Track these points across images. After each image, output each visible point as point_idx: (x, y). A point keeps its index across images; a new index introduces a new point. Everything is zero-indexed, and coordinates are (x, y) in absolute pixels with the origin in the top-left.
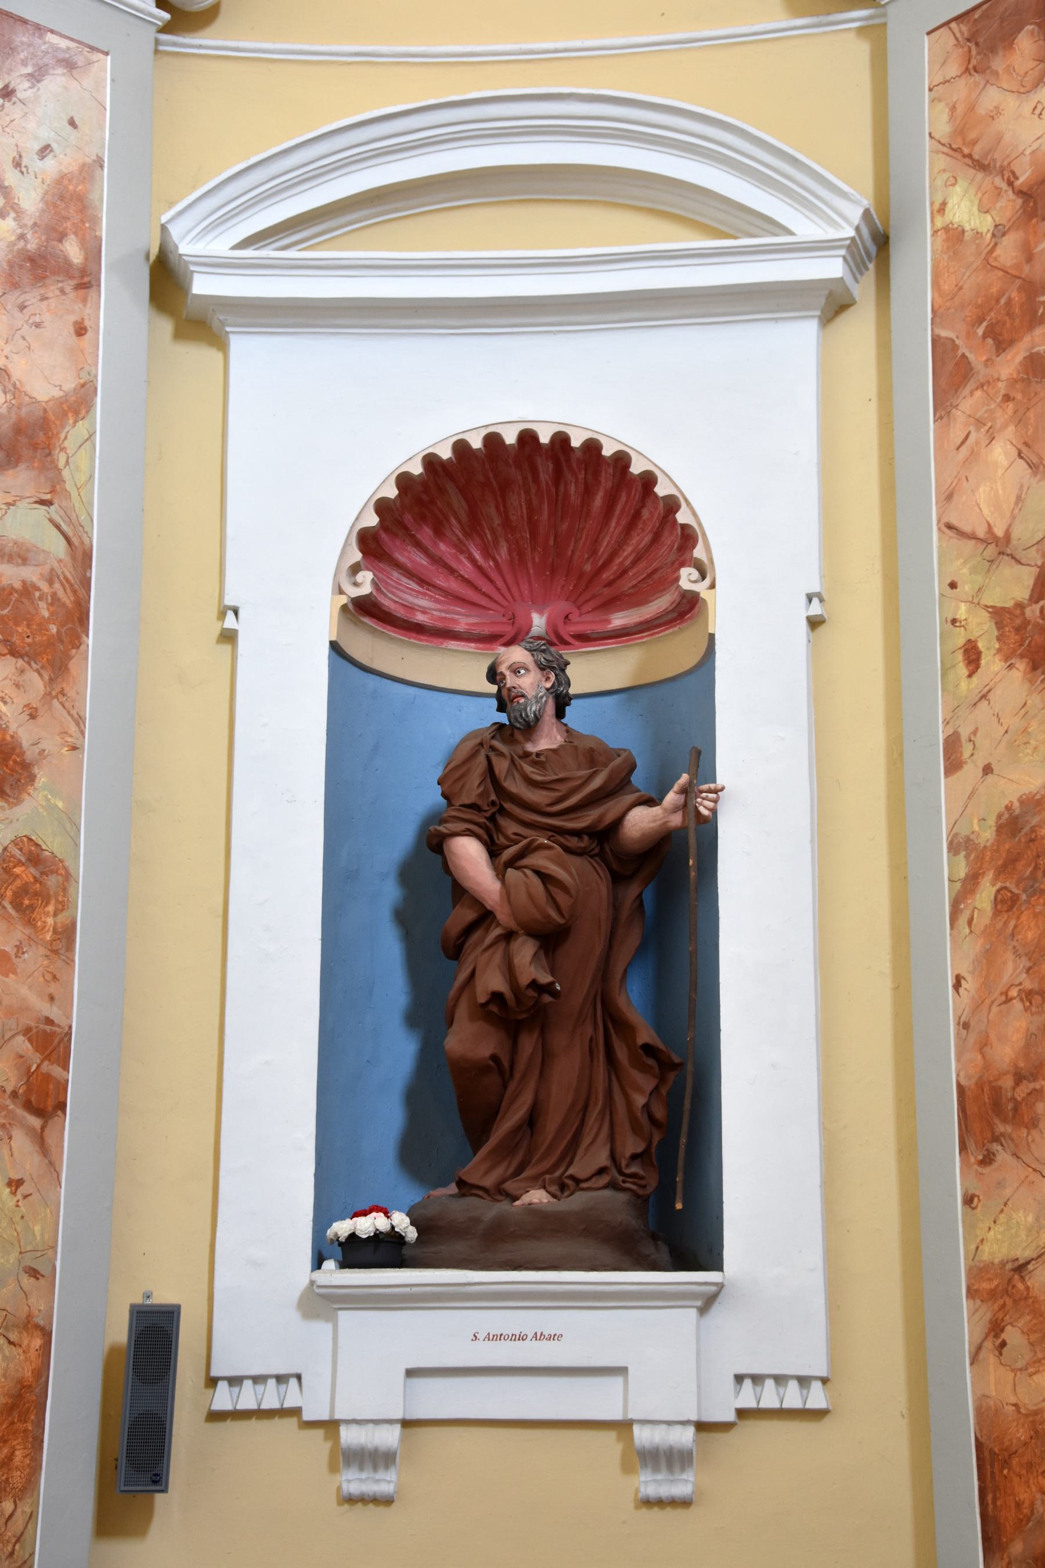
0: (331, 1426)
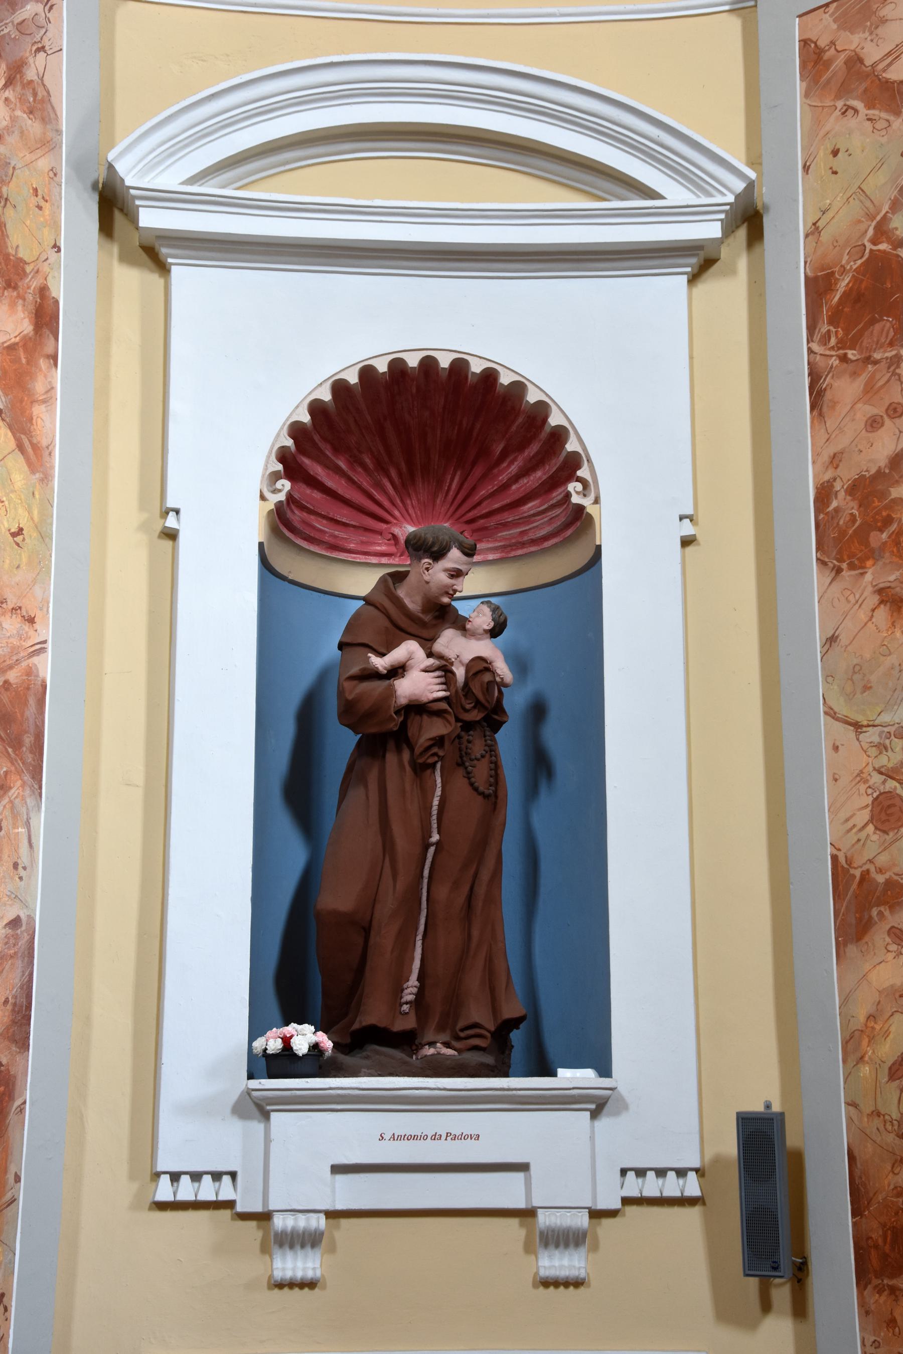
0: (264, 1217)
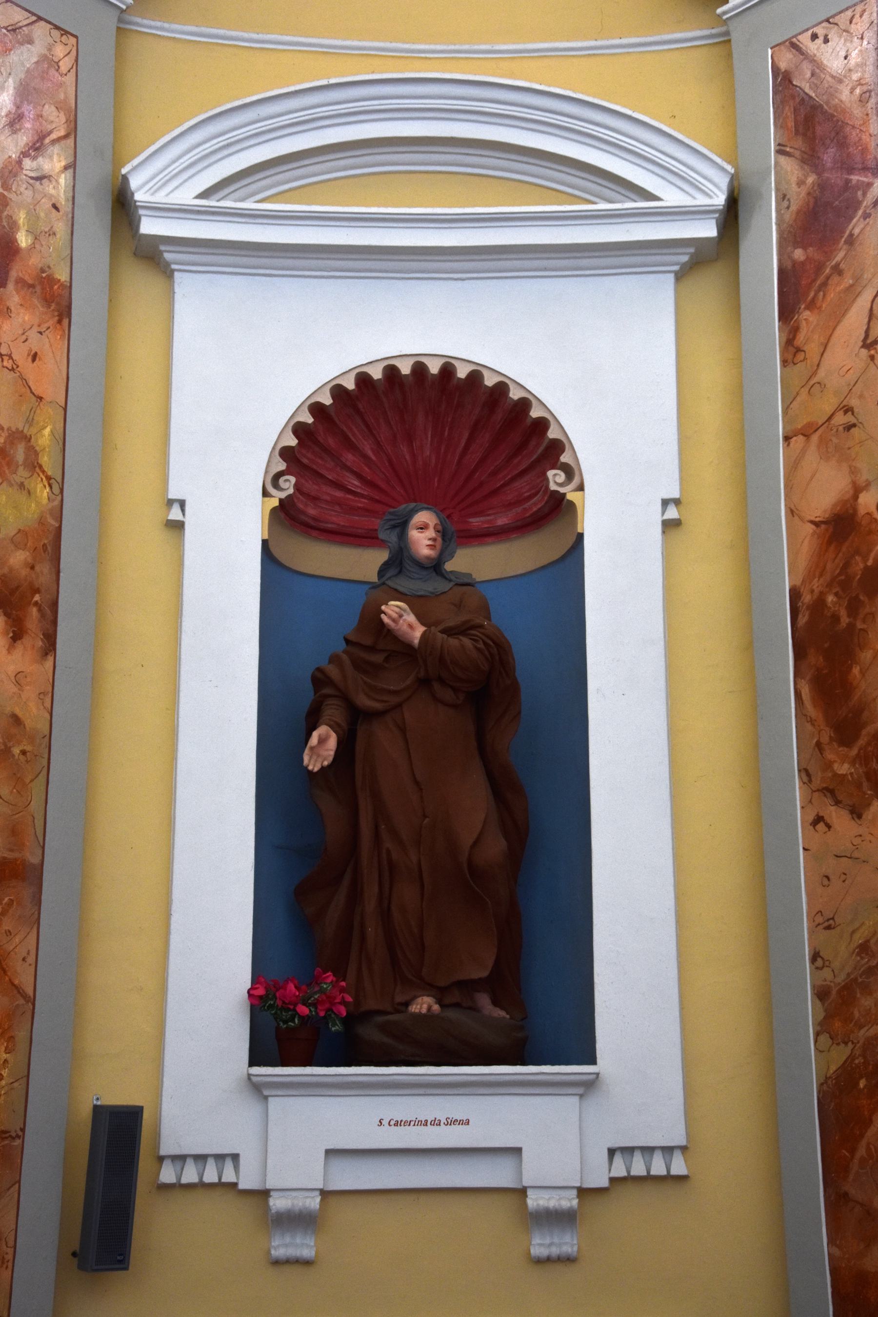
0: (264, 1194)
